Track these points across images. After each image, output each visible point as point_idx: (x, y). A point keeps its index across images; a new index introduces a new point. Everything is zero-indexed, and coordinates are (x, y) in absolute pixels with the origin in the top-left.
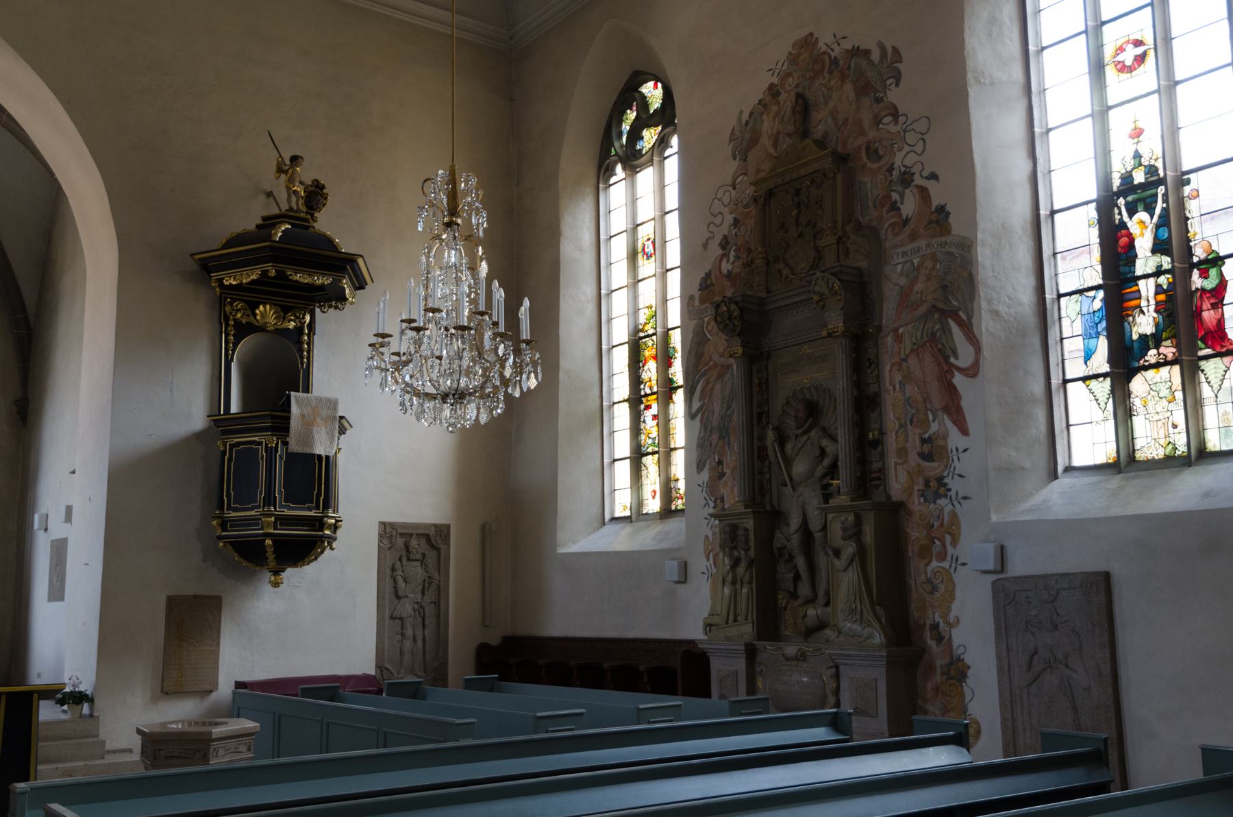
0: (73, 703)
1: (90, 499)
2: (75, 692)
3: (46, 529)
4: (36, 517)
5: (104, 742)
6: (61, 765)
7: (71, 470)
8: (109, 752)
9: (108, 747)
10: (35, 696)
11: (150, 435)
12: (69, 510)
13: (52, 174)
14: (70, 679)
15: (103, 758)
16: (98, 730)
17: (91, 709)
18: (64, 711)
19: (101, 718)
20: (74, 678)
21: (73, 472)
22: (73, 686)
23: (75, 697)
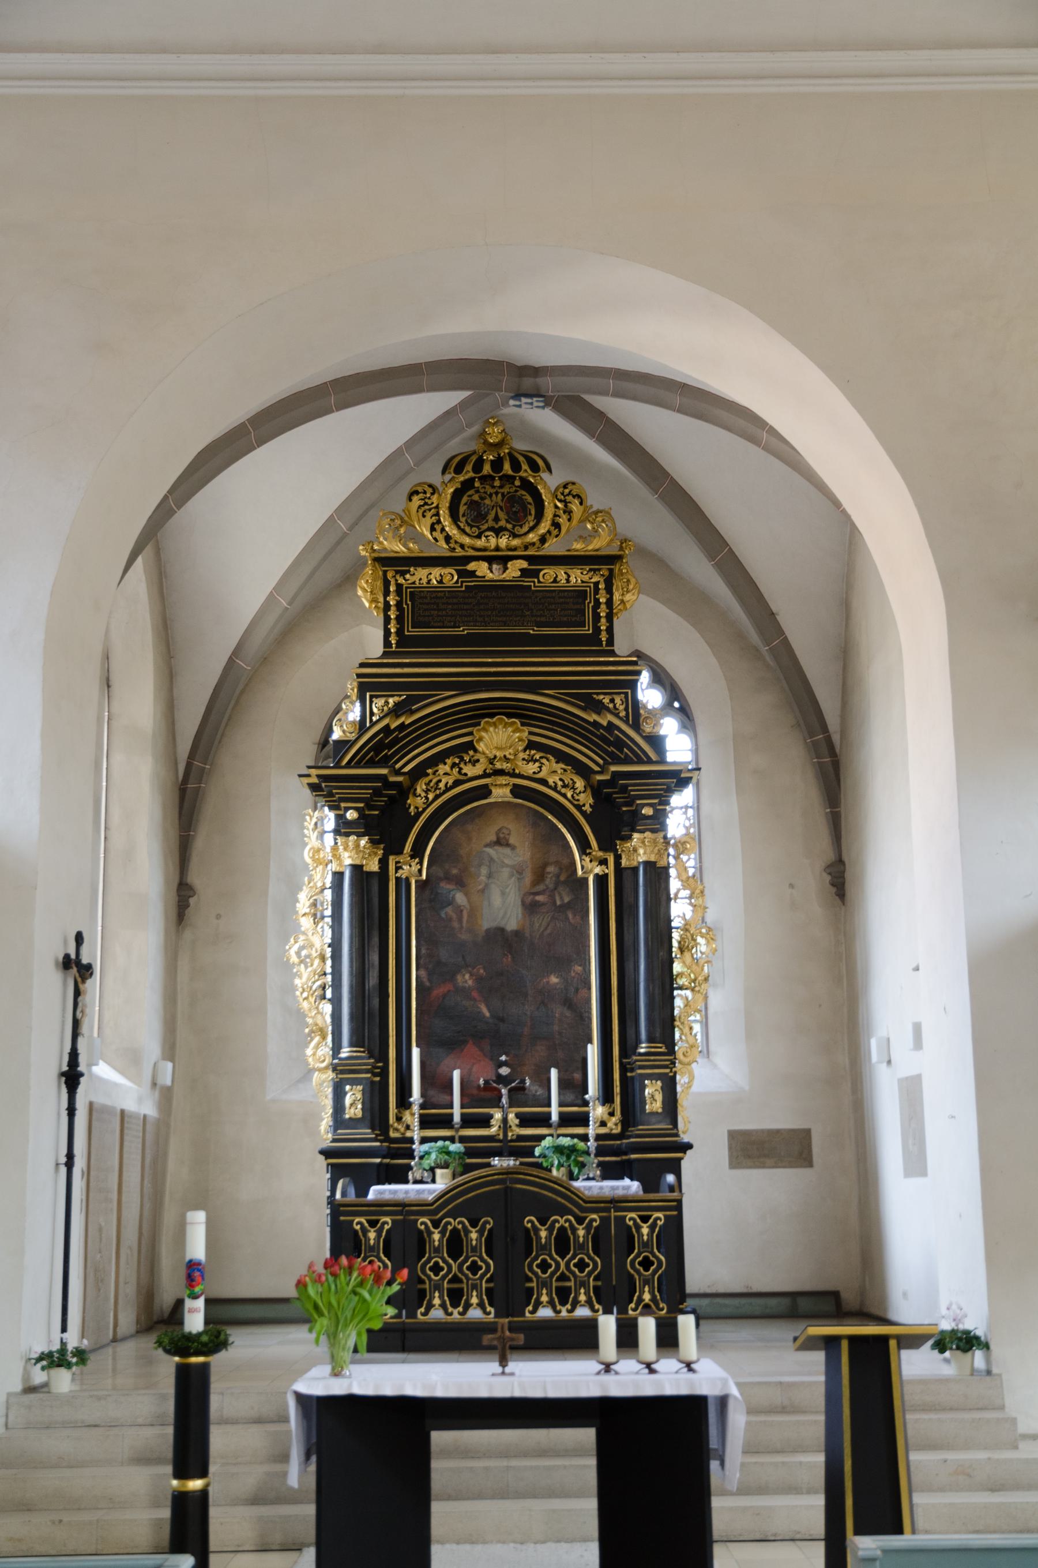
0: (958, 1348)
1: (945, 1009)
2: (958, 1330)
3: (889, 1062)
4: (873, 1042)
5: (1014, 1421)
6: (951, 1456)
7: (914, 965)
8: (1025, 1437)
9: (1022, 1428)
10: (893, 1343)
11: (1027, 896)
12: (917, 1028)
13: (837, 504)
14: (948, 1309)
15: (1016, 1448)
16: (1003, 1398)
17: (988, 1360)
18: (947, 1361)
19: (1004, 1377)
20: (954, 1307)
21: (917, 969)
22: (954, 1320)
23: (960, 1339)
